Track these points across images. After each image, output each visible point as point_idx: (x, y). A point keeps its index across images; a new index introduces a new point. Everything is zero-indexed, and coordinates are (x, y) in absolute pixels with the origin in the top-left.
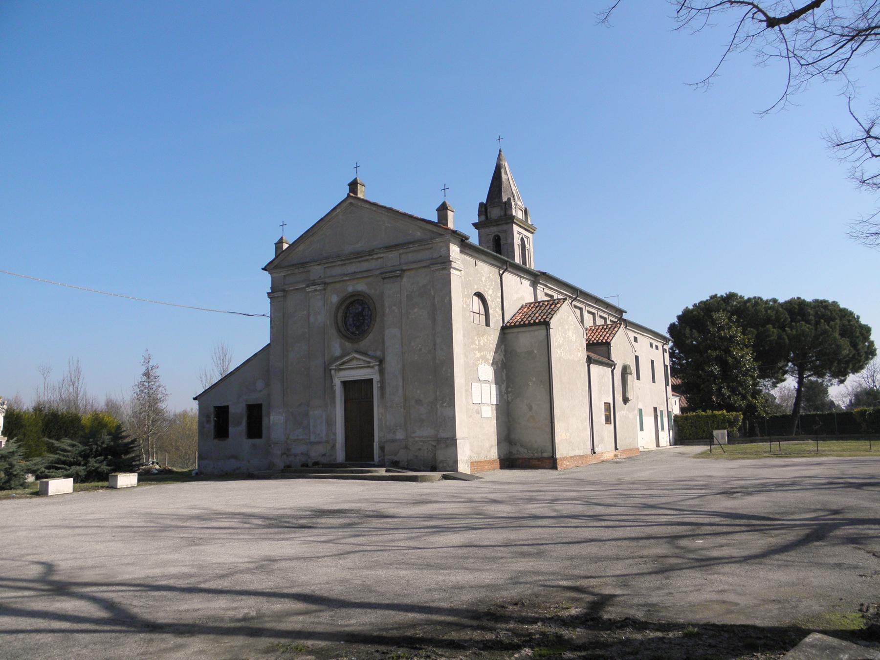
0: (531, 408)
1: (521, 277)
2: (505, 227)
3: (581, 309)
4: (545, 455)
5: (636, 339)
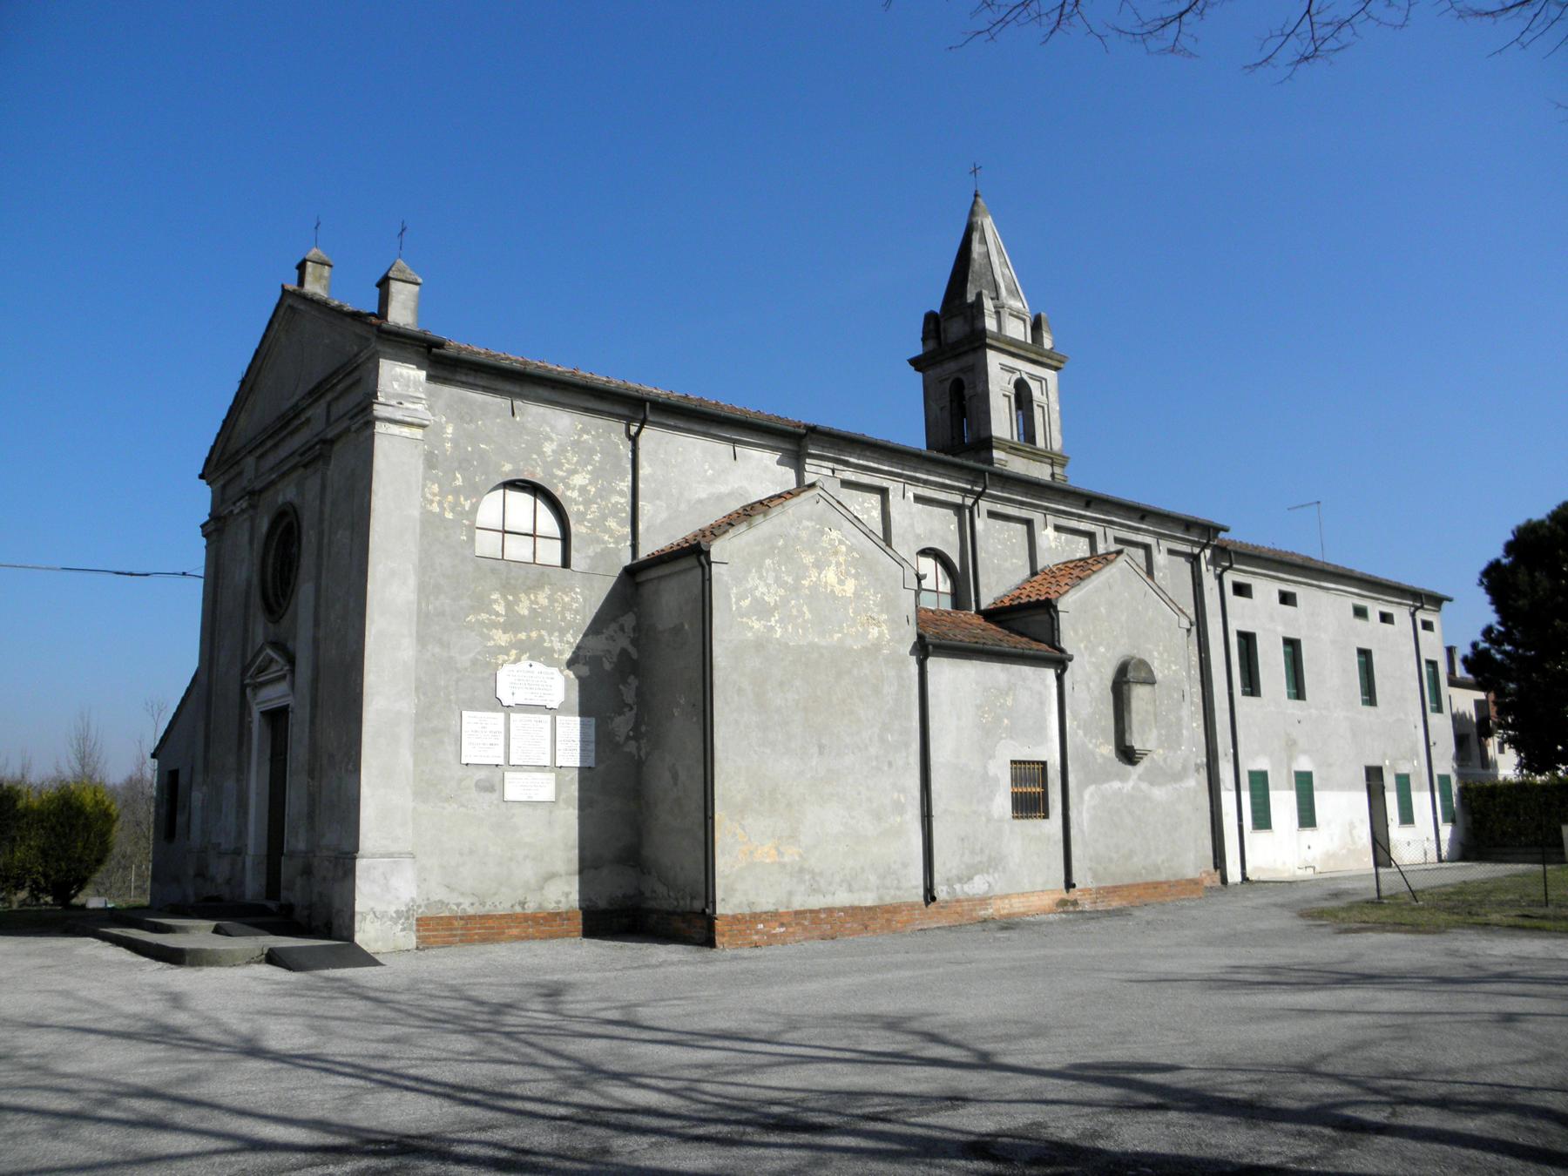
0: (675, 777)
1: (735, 442)
2: (969, 360)
3: (1029, 523)
4: (685, 904)
5: (1287, 599)
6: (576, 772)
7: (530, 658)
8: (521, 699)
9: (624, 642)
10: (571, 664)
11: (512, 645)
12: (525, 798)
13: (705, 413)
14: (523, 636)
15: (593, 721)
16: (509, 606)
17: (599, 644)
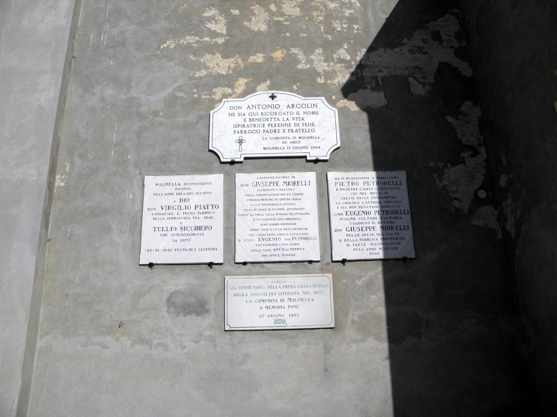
6: (379, 268)
7: (270, 88)
8: (255, 146)
9: (443, 54)
10: (348, 91)
11: (238, 73)
12: (267, 323)
13: (75, 9)
14: (259, 58)
15: (401, 176)
16: (232, 22)
17: (397, 60)
